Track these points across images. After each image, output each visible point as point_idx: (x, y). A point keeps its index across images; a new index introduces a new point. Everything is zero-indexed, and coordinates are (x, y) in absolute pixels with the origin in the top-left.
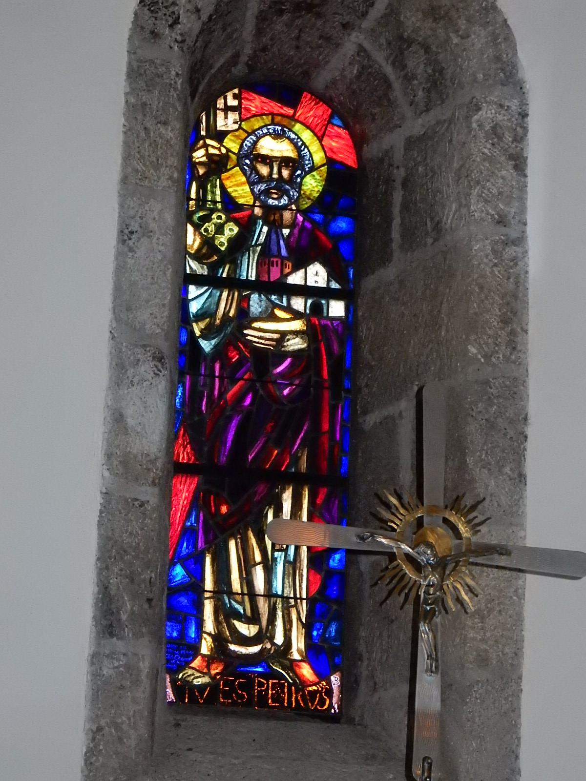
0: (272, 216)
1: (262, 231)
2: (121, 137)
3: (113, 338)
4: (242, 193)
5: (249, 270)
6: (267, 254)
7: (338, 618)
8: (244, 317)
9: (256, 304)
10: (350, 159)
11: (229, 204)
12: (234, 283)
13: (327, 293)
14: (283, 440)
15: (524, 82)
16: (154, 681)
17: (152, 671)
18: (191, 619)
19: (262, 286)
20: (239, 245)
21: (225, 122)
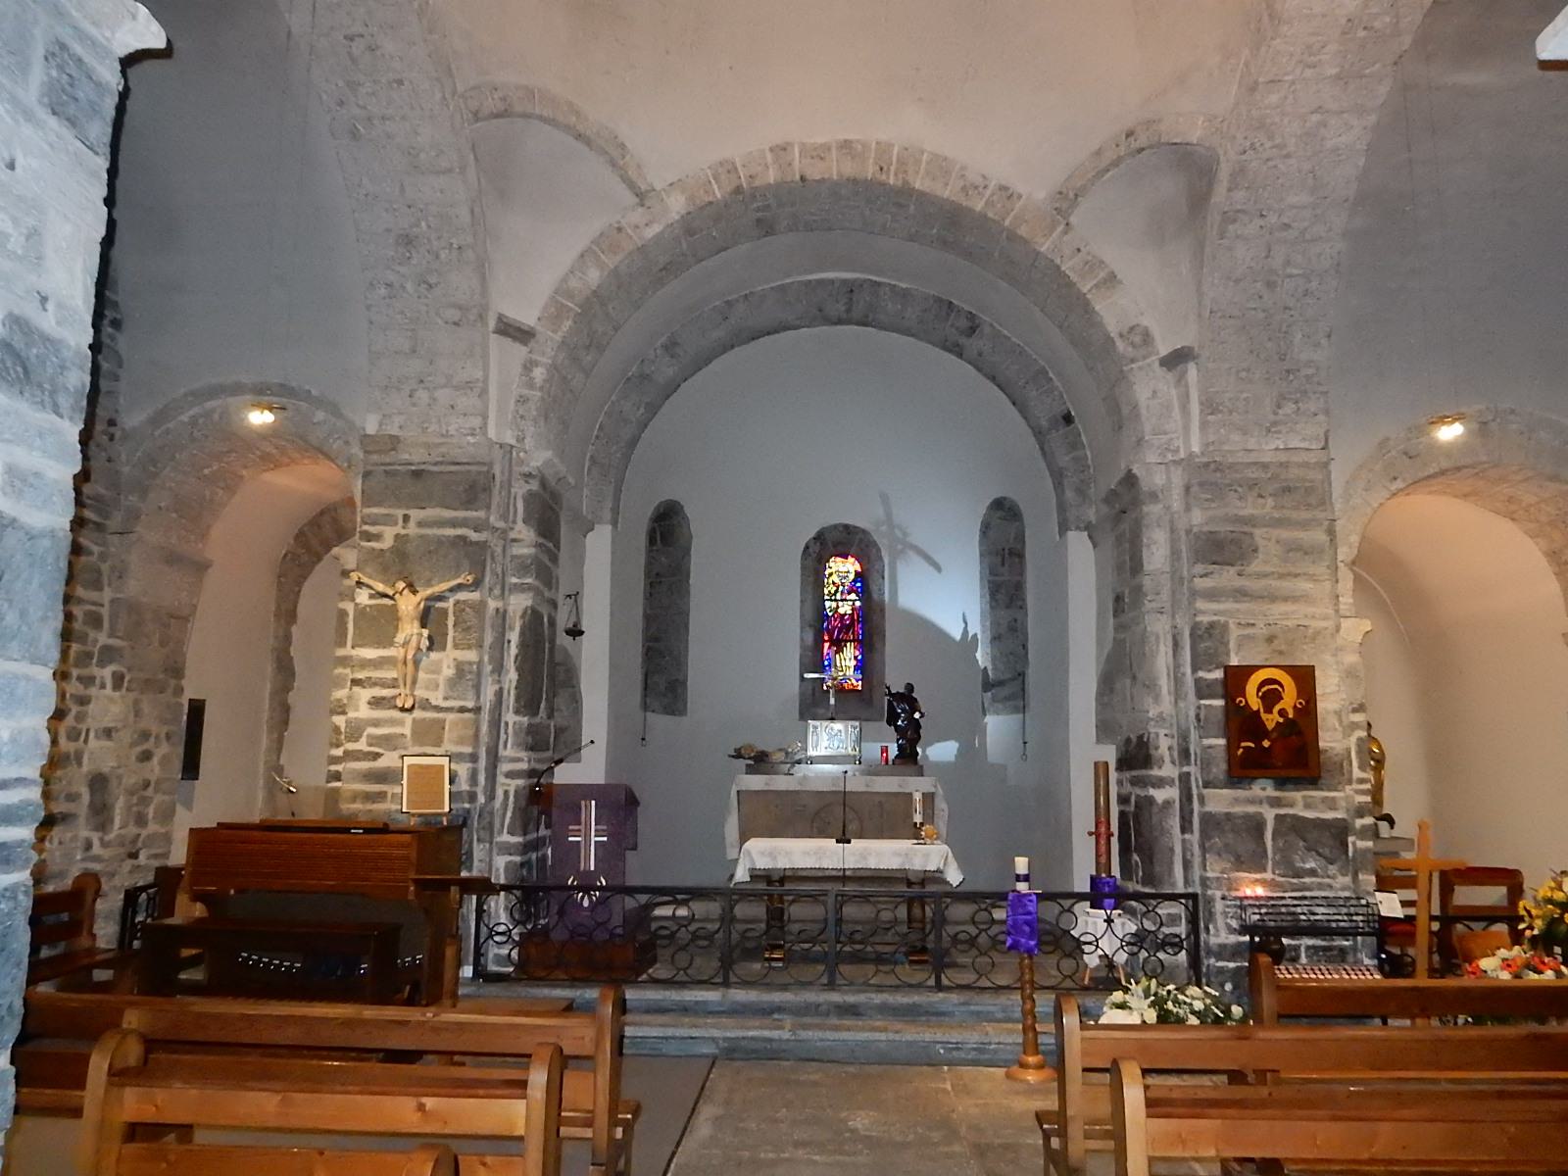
0: (843, 584)
1: (841, 588)
2: (607, 681)
3: (1465, 496)
4: (837, 581)
5: (838, 597)
6: (842, 593)
7: (522, 966)
8: (838, 607)
9: (840, 603)
10: (860, 570)
11: (834, 583)
12: (836, 600)
13: (854, 601)
14: (847, 633)
15: (634, 848)
16: (812, 1074)
17: (784, 1051)
18: (805, 777)
19: (842, 600)
20: (836, 591)
21: (832, 564)
